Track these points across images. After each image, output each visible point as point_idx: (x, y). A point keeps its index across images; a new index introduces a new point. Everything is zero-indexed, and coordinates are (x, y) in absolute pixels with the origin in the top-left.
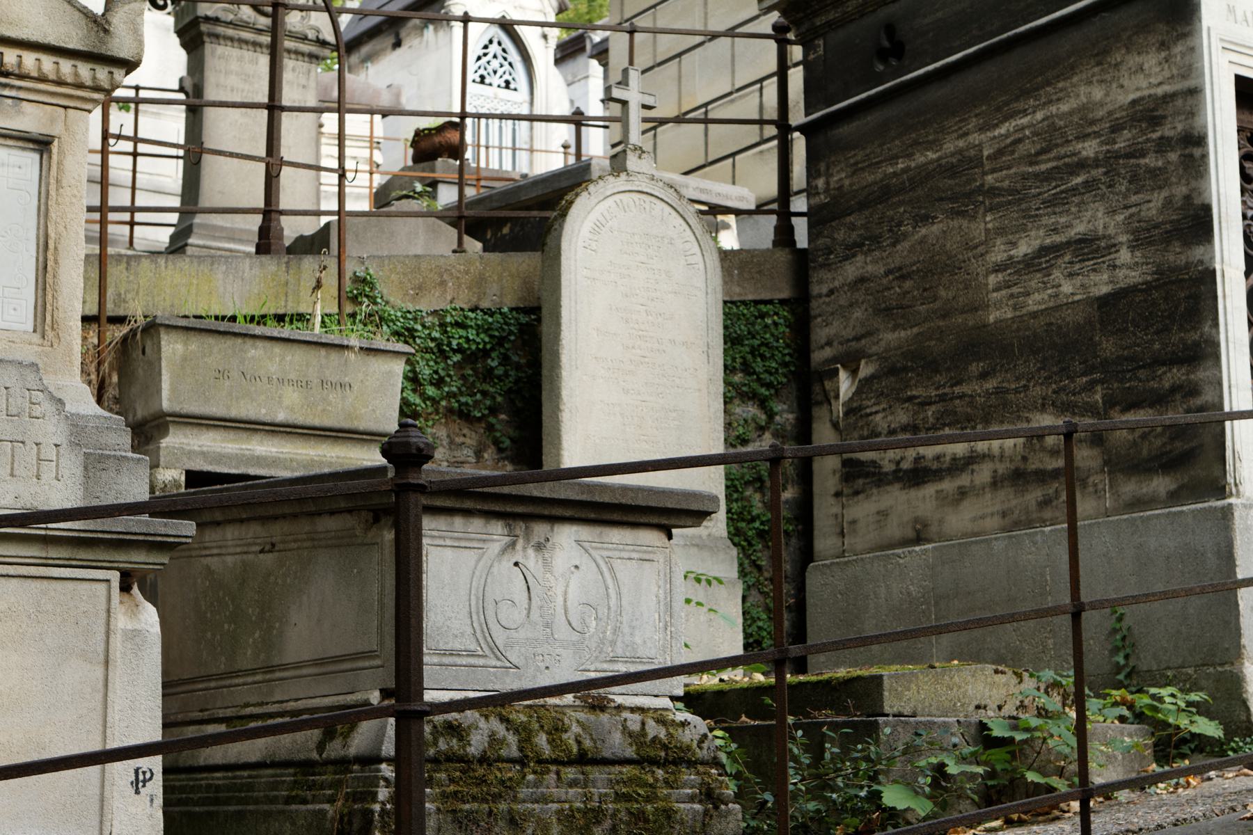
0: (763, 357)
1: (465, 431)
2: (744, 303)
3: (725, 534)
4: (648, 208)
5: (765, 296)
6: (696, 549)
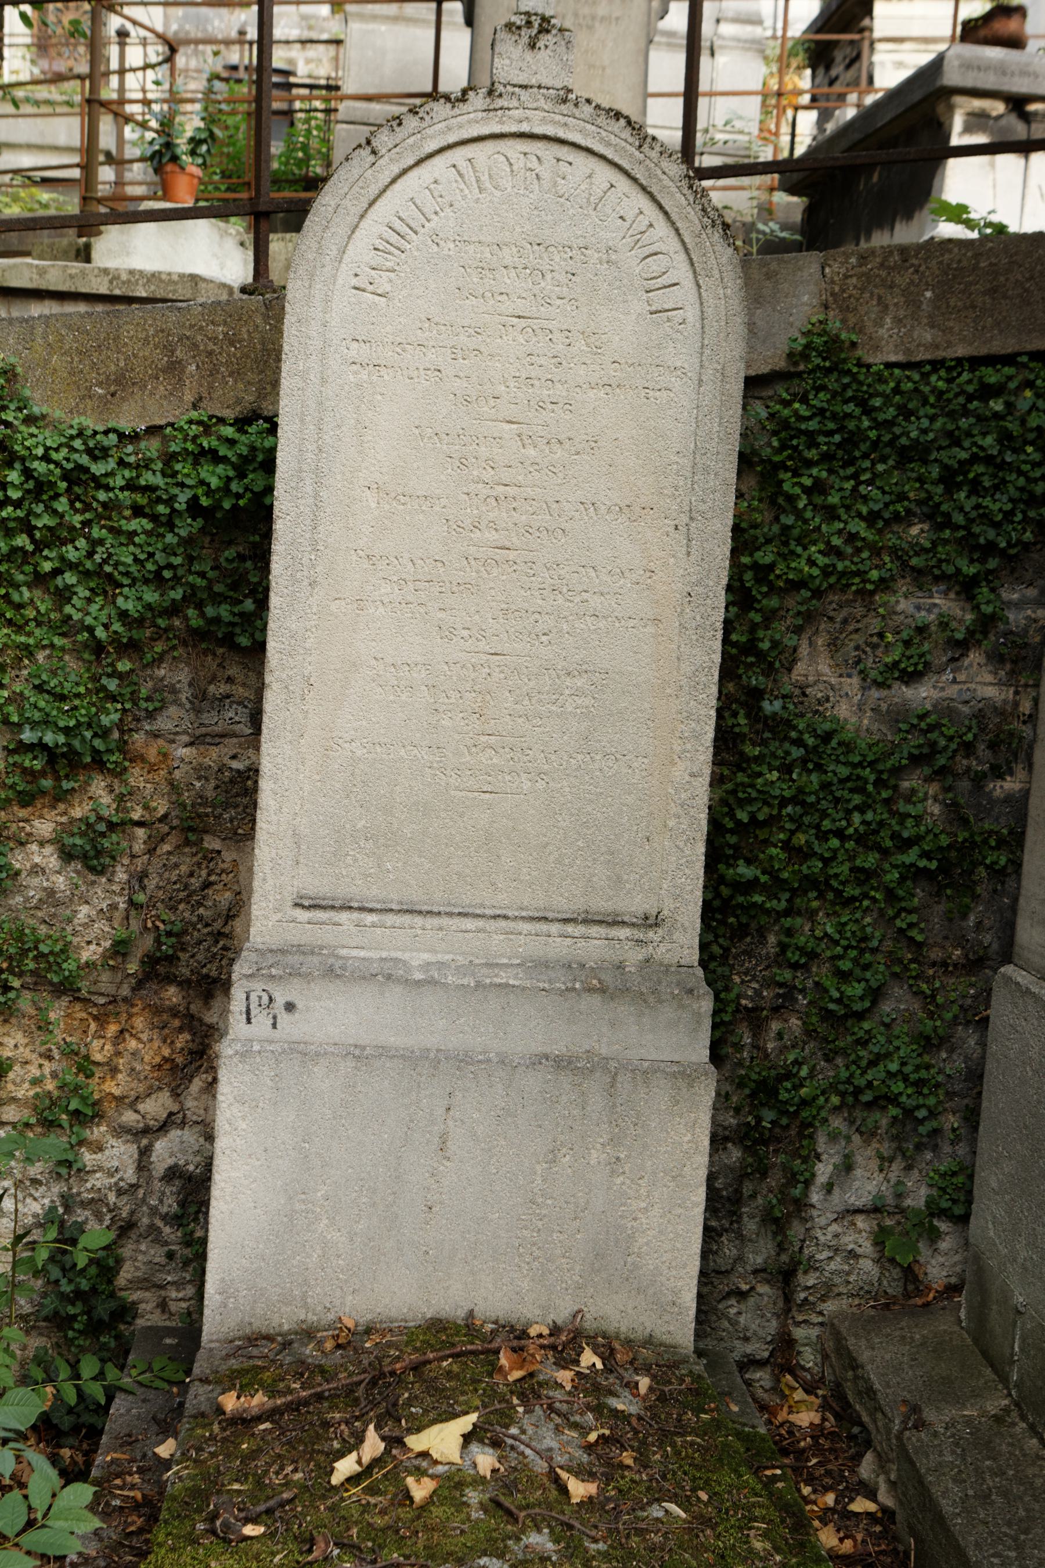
0: (975, 488)
1: (233, 671)
2: (937, 365)
3: (692, 955)
4: (546, 175)
5: (1000, 345)
6: (596, 1000)
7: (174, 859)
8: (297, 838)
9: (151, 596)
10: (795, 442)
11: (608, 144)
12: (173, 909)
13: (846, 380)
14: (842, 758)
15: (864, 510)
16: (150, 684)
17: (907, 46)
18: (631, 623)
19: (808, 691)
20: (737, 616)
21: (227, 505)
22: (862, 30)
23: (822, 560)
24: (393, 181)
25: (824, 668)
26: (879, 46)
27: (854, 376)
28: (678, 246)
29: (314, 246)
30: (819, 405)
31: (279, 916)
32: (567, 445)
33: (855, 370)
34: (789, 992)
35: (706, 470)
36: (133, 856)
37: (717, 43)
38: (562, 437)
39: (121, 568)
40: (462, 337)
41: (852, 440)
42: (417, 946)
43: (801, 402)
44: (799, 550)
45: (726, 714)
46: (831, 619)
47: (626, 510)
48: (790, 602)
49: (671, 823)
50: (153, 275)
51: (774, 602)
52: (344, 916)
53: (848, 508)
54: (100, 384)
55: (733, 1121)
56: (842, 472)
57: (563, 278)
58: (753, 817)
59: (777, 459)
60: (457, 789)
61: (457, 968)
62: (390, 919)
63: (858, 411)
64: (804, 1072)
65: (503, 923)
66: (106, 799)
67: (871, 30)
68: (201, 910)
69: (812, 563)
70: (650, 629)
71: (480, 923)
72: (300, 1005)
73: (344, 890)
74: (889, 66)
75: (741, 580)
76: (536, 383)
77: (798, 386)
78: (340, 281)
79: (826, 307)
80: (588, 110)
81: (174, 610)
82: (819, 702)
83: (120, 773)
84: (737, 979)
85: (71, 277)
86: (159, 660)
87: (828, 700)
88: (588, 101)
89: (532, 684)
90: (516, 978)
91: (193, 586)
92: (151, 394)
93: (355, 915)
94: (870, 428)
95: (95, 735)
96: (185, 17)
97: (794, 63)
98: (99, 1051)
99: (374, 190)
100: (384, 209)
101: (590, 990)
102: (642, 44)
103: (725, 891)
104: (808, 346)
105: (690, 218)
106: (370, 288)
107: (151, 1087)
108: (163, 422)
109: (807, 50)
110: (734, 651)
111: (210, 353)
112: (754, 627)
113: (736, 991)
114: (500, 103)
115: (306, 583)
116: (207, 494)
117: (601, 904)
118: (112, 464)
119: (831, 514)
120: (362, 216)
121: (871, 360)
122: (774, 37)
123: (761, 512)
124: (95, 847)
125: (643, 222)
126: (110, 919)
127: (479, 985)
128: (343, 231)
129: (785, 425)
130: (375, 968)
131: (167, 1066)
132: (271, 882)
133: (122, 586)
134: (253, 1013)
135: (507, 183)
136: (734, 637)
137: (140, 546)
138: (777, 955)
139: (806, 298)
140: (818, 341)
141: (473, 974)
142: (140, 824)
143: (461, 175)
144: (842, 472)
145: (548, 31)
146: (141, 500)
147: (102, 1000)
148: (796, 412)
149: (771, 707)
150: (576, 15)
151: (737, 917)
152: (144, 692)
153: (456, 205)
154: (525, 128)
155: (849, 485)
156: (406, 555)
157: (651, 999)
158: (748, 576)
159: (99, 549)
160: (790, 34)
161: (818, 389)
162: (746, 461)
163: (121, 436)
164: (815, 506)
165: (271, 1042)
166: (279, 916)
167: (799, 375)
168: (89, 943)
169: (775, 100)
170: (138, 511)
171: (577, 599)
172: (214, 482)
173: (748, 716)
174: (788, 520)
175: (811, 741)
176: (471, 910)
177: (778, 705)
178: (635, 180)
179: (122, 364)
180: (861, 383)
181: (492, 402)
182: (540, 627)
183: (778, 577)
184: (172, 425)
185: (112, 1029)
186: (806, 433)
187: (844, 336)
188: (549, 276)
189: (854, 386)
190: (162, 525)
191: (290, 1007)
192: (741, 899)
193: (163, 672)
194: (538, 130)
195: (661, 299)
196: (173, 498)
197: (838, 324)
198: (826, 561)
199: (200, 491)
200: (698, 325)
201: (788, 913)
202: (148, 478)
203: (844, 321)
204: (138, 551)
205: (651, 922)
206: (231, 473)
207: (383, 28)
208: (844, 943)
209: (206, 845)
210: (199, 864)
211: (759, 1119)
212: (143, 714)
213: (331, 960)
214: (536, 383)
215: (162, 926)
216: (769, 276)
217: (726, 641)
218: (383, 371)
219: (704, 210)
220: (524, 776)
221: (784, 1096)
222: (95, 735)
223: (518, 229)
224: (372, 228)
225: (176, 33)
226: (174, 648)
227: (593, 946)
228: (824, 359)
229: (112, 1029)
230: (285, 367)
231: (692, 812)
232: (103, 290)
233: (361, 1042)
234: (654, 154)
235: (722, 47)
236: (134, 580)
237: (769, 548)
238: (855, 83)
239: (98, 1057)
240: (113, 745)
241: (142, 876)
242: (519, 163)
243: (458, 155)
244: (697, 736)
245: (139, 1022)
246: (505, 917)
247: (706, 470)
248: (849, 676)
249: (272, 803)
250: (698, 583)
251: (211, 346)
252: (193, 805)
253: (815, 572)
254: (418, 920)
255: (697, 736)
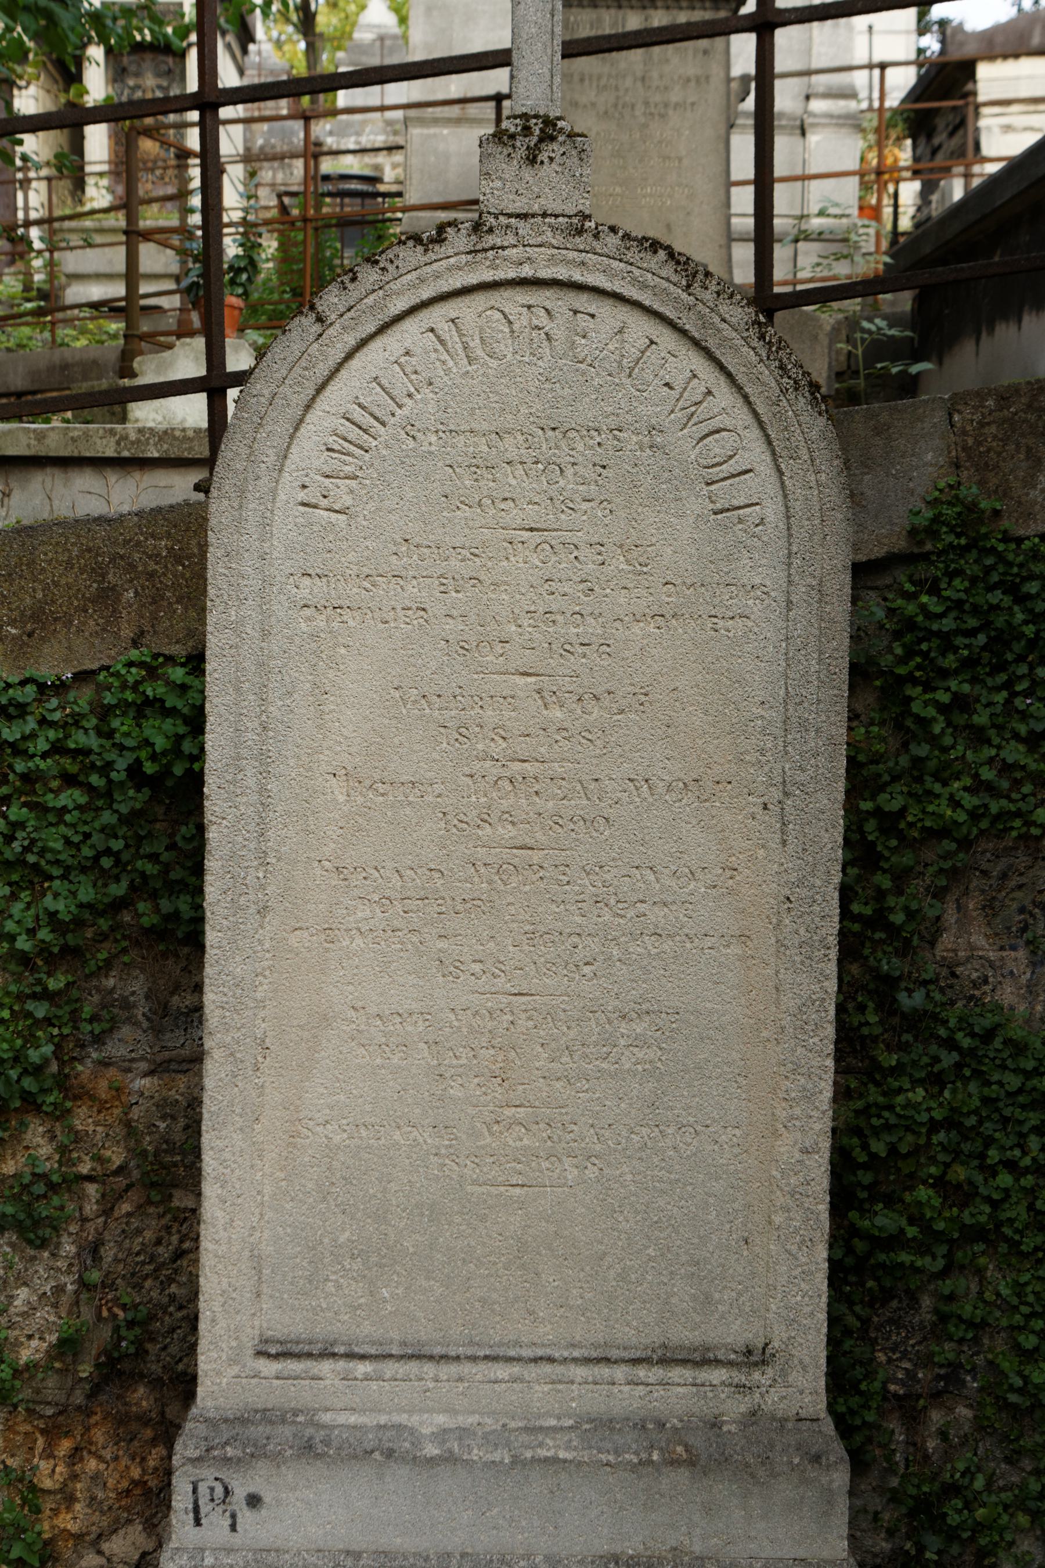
4: (559, 334)
6: (683, 1475)
7: (135, 1223)
8: (257, 1261)
9: (86, 894)
10: (924, 646)
11: (644, 286)
12: (138, 1287)
13: (989, 561)
14: (1009, 1062)
15: (1023, 729)
16: (96, 998)
17: (1015, 108)
18: (709, 942)
19: (959, 970)
20: (859, 878)
21: (178, 770)
22: (965, 96)
23: (969, 801)
24: (349, 356)
25: (978, 939)
26: (985, 111)
27: (1001, 558)
28: (749, 419)
29: (244, 451)
30: (955, 596)
31: (235, 1370)
32: (606, 700)
33: (1001, 547)
34: (953, 1374)
35: (803, 725)
36: (84, 1220)
37: (808, 121)
38: (599, 690)
39: (49, 856)
40: (453, 562)
41: (1001, 640)
42: (426, 1405)
43: (929, 593)
44: (937, 788)
45: (850, 1006)
46: (985, 873)
47: (693, 786)
48: (928, 855)
49: (778, 1219)
50: (165, 432)
51: (907, 859)
52: (326, 1367)
53: (1000, 728)
54: (13, 623)
55: (886, 1546)
56: (990, 682)
57: (590, 473)
58: (893, 1150)
59: (901, 670)
60: (475, 1182)
61: (485, 1436)
62: (390, 1368)
63: (1007, 601)
64: (979, 1483)
65: (547, 1368)
66: (45, 1150)
67: (974, 94)
68: (173, 1289)
69: (955, 803)
70: (735, 950)
71: (516, 1369)
72: (267, 1497)
73: (324, 1329)
74: (996, 130)
75: (861, 830)
76: (559, 618)
77: (922, 571)
78: (282, 496)
79: (958, 466)
80: (612, 241)
81: (119, 905)
82: (975, 985)
83: (62, 1114)
84: (881, 1357)
85: (73, 440)
86: (108, 965)
87: (986, 981)
88: (613, 229)
89: (572, 1034)
90: (568, 1448)
91: (143, 874)
92: (79, 631)
93: (341, 1364)
94: (1026, 622)
95: (25, 1072)
96: (270, 131)
97: (893, 135)
98: (49, 1474)
99: (322, 370)
100: (337, 394)
101: (675, 1463)
102: (722, 129)
103: (860, 1246)
104: (936, 519)
105: (764, 380)
106: (324, 503)
107: (117, 1520)
108: (95, 666)
109: (906, 120)
110: (856, 927)
111: (151, 575)
112: (881, 894)
113: (881, 1375)
114: (490, 240)
115: (253, 909)
116: (154, 757)
117: (683, 1334)
118: (31, 724)
119: (978, 737)
120: (308, 407)
121: (1021, 532)
122: (870, 109)
123: (884, 740)
124: (30, 1216)
125: (698, 389)
126: (55, 1306)
127: (516, 1461)
128: (283, 428)
129: (910, 624)
130: (370, 1440)
131: (138, 1491)
132: (222, 1324)
133: (51, 878)
134: (203, 1510)
135: (505, 347)
136: (856, 908)
137: (73, 826)
138: (934, 1324)
139: (929, 456)
140: (949, 512)
141: (508, 1445)
142: (89, 1178)
143: (442, 342)
144: (990, 682)
145: (553, 139)
146: (72, 768)
147: (49, 1411)
148: (923, 607)
149: (911, 1000)
150: (647, 104)
151: (877, 1279)
152: (87, 1011)
153: (437, 381)
154: (527, 271)
155: (1001, 697)
156: (390, 865)
157: (761, 1473)
158: (871, 826)
159: (20, 834)
160: (888, 104)
161: (952, 575)
162: (860, 673)
163: (42, 687)
164: (955, 728)
165: (230, 1551)
166: (235, 1370)
167: (925, 557)
168: (30, 1337)
169: (877, 177)
170: (69, 780)
171: (631, 913)
172: (160, 743)
173: (879, 1008)
174: (922, 750)
175: (966, 1042)
176: (501, 1352)
177: (919, 996)
178: (683, 332)
179: (40, 595)
180: (1010, 564)
181: (499, 649)
182: (581, 954)
183: (911, 825)
184: (107, 668)
185: (65, 1446)
186: (938, 634)
187: (983, 505)
188: (569, 471)
189: (1001, 568)
190: (100, 796)
191: (254, 1501)
192: (882, 1257)
193: (111, 982)
194: (544, 274)
195: (728, 493)
196: (109, 765)
197: (974, 490)
198: (976, 801)
199: (143, 754)
200: (782, 526)
201: (944, 1273)
202: (79, 739)
203: (982, 483)
204: (69, 833)
205: (755, 1357)
206: (182, 730)
207: (445, 132)
208: (1025, 1309)
209: (176, 1203)
210: (168, 1228)
211: (921, 1549)
212: (88, 1038)
213: (309, 1431)
214: (559, 618)
215: (121, 1314)
216: (878, 431)
217: (845, 913)
218: (347, 615)
219: (782, 367)
220: (567, 1162)
221: (954, 1519)
222: (25, 1072)
223: (524, 410)
224: (322, 421)
225: (262, 148)
226: (124, 951)
227: (677, 1394)
228: (958, 536)
229: (65, 1446)
230: (211, 619)
231: (807, 1203)
232: (110, 453)
233: (355, 1547)
234: (708, 296)
235: (813, 125)
236: (68, 869)
237: (897, 787)
238: (960, 154)
239: (48, 1484)
240: (49, 1083)
241: (95, 1249)
242: (522, 321)
243: (436, 315)
244: (808, 1097)
245: (99, 1436)
246: (551, 1360)
247: (803, 725)
248: (1014, 948)
249: (219, 1214)
250: (800, 883)
251: (152, 566)
252: (156, 1155)
253: (962, 817)
254: (429, 1369)
255: (808, 1097)
